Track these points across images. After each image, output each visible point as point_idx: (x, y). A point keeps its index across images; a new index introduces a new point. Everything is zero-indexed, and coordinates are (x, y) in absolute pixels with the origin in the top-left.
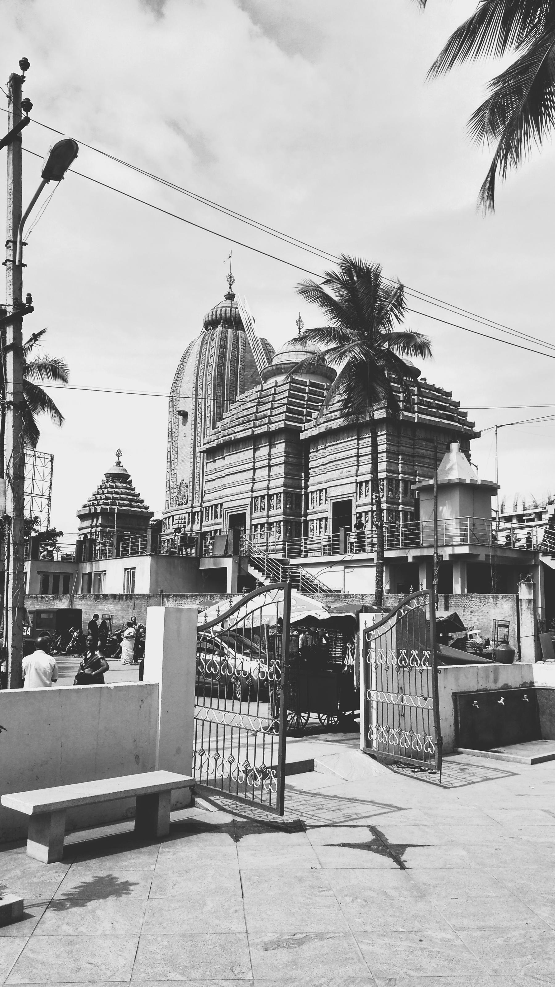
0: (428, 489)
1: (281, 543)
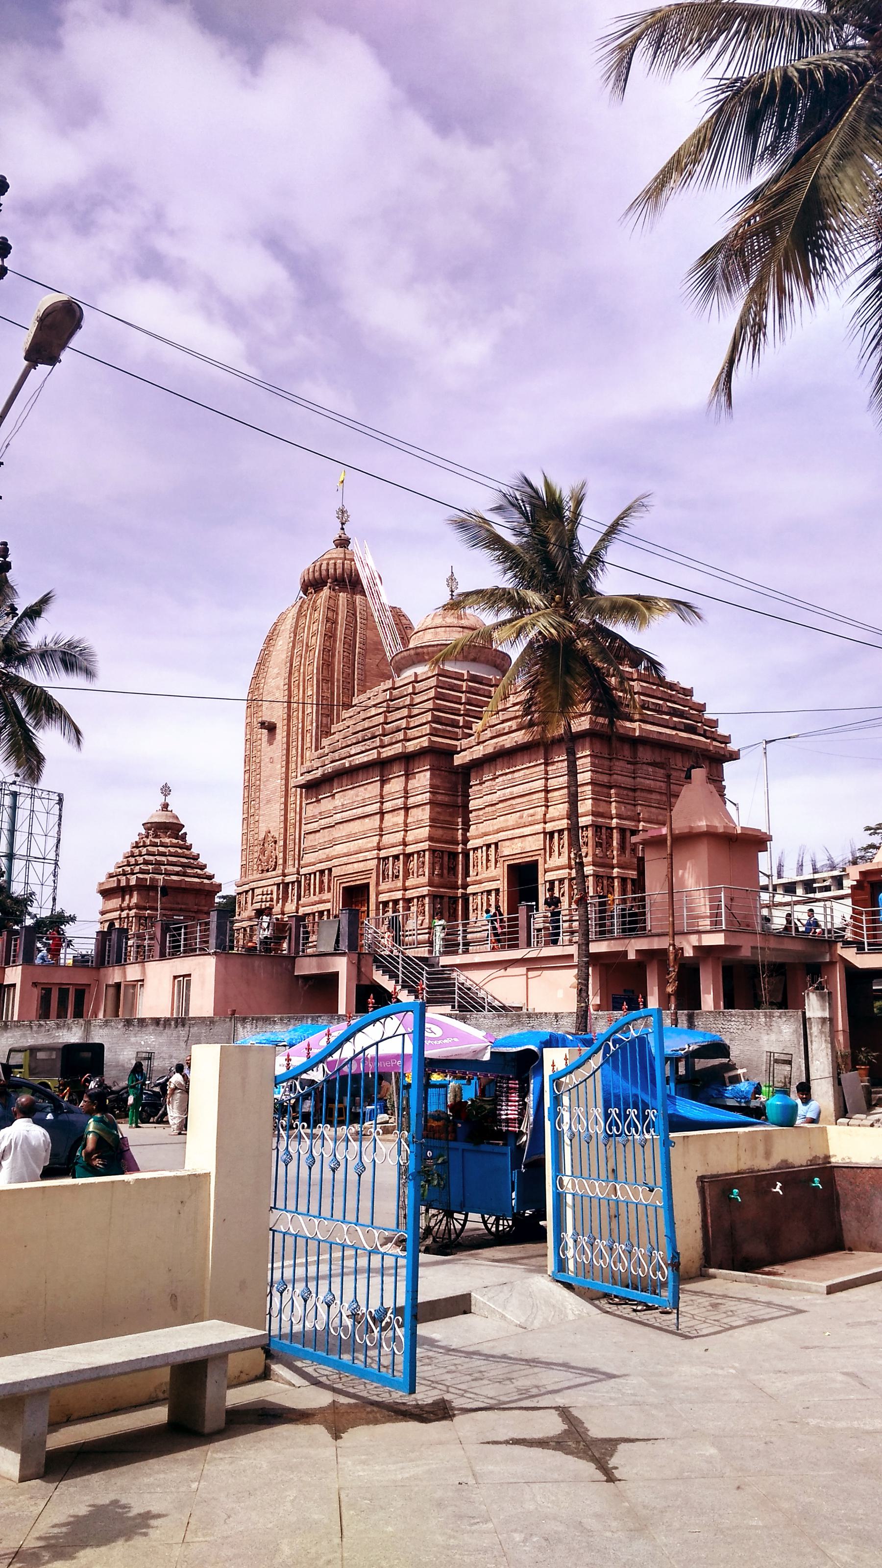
0: (658, 842)
1: (426, 931)
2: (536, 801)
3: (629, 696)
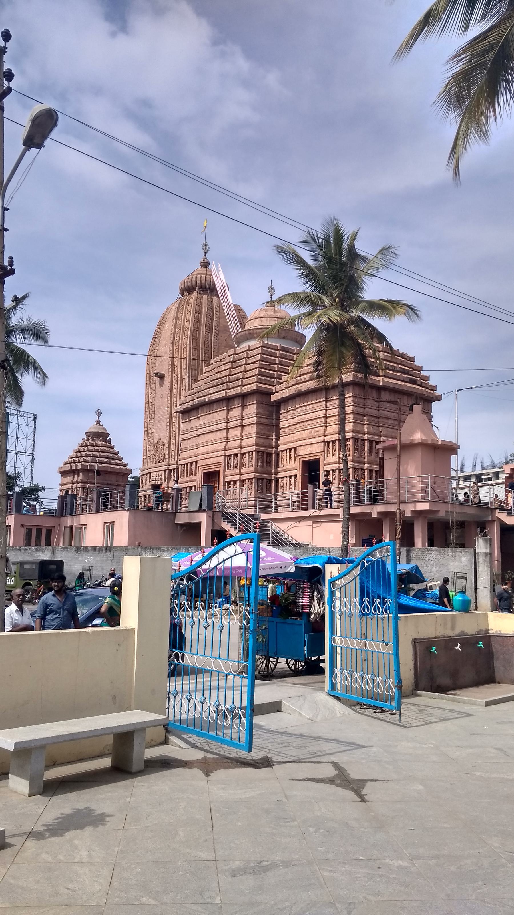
0: (392, 448)
1: (253, 499)
2: (320, 423)
3: (378, 362)
